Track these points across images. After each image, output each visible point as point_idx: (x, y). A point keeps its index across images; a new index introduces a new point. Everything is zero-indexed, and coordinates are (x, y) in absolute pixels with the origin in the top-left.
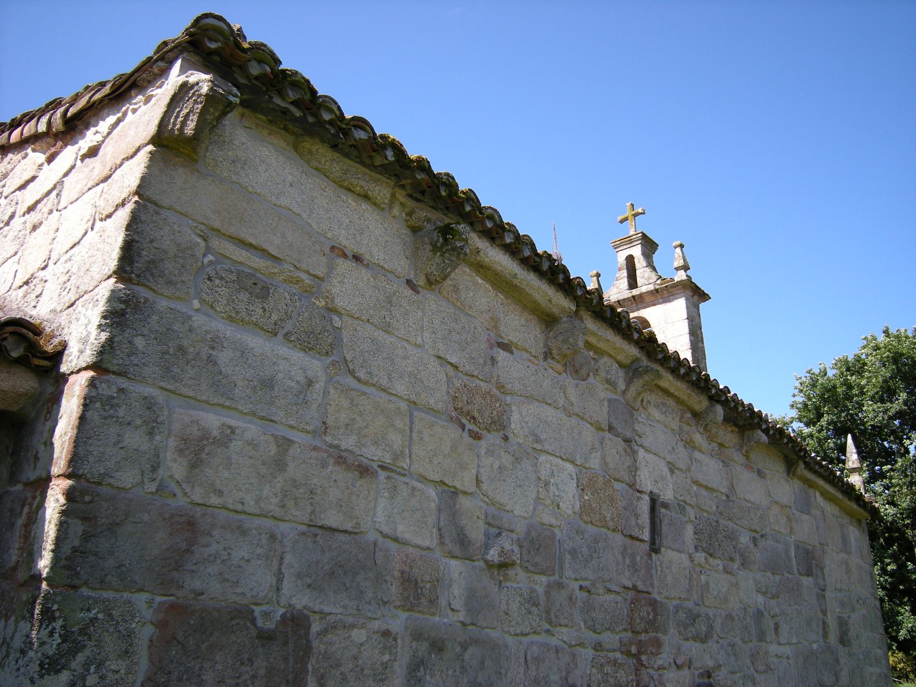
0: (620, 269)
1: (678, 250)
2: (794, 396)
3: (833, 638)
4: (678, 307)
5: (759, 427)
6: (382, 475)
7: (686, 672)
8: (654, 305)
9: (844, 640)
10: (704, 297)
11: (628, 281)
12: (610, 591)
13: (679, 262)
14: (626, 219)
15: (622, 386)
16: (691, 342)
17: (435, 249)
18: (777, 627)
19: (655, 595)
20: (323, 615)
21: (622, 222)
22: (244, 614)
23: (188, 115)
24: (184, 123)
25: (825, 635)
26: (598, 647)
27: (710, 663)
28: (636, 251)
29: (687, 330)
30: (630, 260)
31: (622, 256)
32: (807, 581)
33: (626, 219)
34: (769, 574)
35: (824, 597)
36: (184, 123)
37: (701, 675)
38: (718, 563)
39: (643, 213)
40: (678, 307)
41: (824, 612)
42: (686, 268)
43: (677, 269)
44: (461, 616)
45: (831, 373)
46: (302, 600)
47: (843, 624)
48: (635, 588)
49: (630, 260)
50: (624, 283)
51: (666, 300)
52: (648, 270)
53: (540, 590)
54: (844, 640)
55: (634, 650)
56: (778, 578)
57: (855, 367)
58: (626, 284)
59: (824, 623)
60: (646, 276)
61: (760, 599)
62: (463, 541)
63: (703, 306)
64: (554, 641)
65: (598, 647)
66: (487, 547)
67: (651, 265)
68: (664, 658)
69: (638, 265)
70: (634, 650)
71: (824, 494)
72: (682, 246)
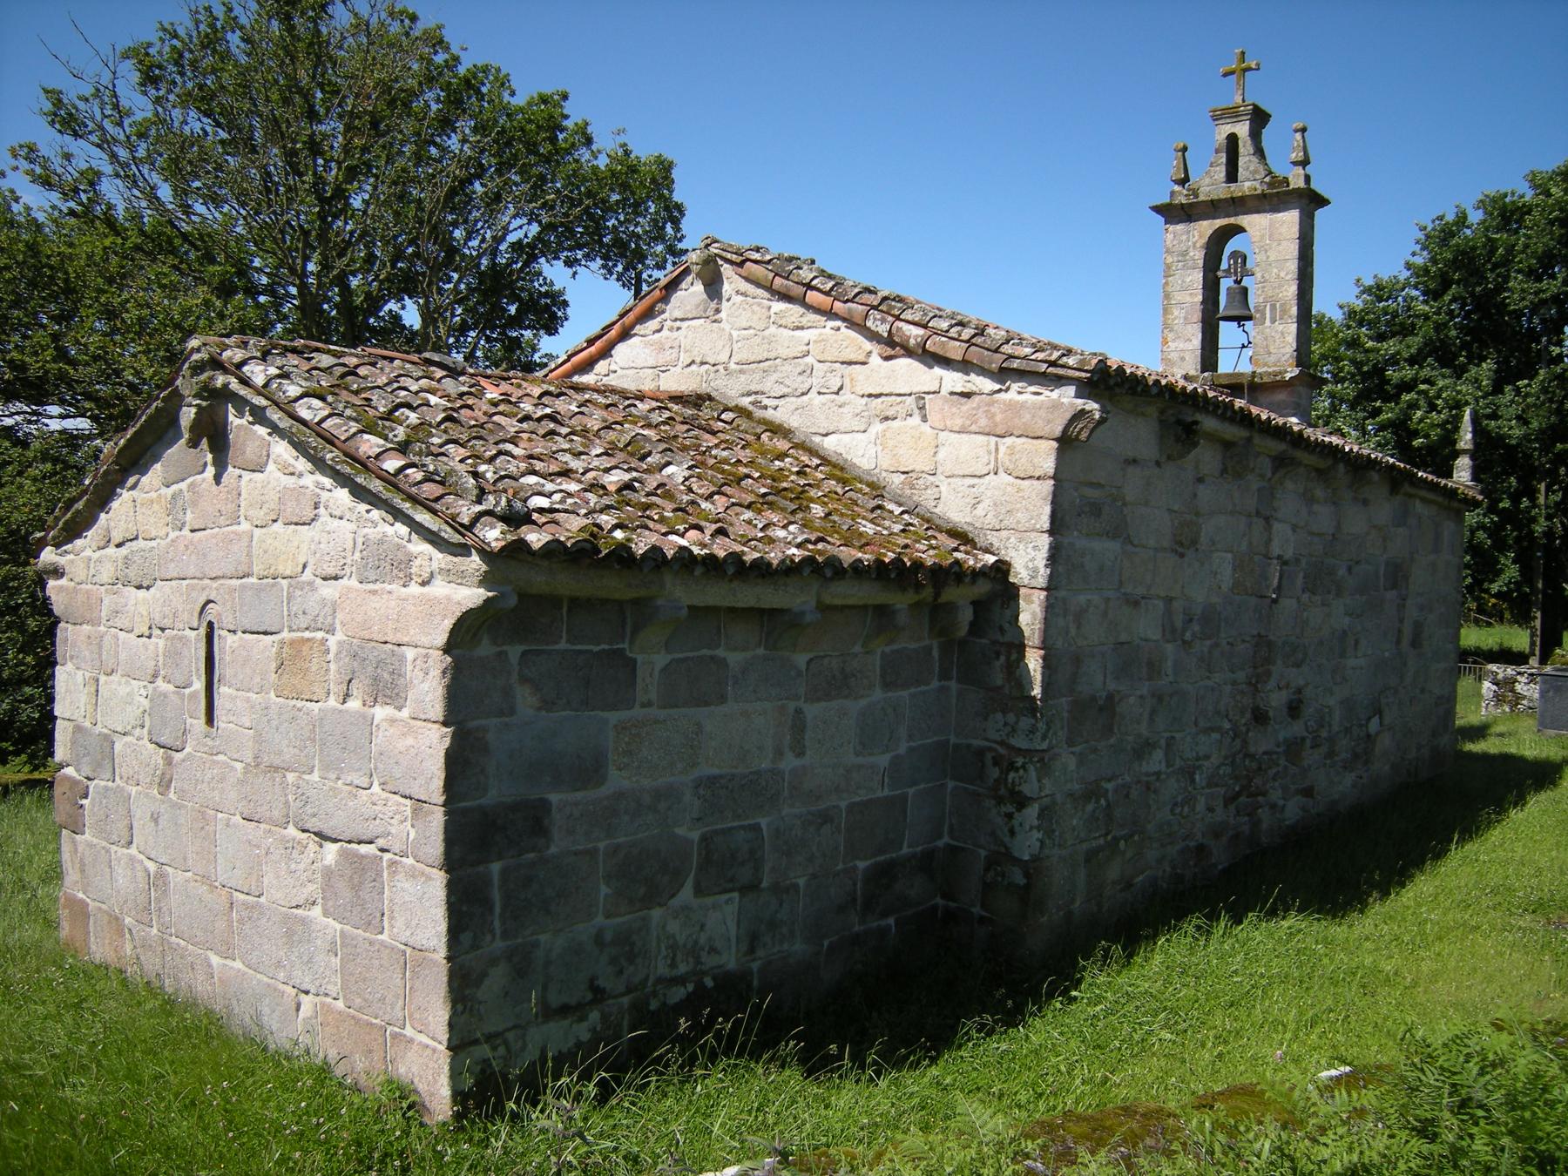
0: (1217, 151)
1: (1298, 136)
2: (1414, 254)
3: (1405, 642)
4: (1289, 220)
5: (1373, 468)
6: (1143, 602)
7: (1284, 692)
8: (1258, 212)
9: (1415, 643)
10: (1320, 201)
11: (1227, 171)
12: (1243, 641)
13: (1298, 155)
14: (1232, 73)
15: (1269, 475)
16: (1299, 268)
17: (1178, 440)
18: (1357, 642)
19: (1272, 637)
20: (1119, 692)
21: (1225, 75)
22: (1093, 699)
23: (1082, 429)
24: (1079, 433)
25: (1398, 642)
26: (1234, 683)
27: (1302, 682)
28: (1242, 129)
29: (1296, 253)
30: (1232, 140)
31: (1226, 129)
32: (1391, 595)
33: (1232, 73)
34: (1358, 597)
35: (1404, 606)
36: (1079, 433)
37: (1294, 693)
38: (1318, 598)
39: (1258, 69)
40: (1289, 220)
41: (1401, 621)
42: (1305, 163)
43: (1295, 163)
44: (1171, 679)
45: (1475, 217)
46: (1112, 686)
47: (1418, 627)
48: (1259, 635)
49: (1232, 140)
50: (1220, 173)
51: (1276, 209)
52: (1255, 159)
53: (1205, 650)
54: (1415, 643)
55: (1254, 681)
56: (1364, 598)
57: (1506, 214)
58: (1223, 174)
59: (1400, 631)
60: (1252, 168)
61: (1347, 620)
62: (1173, 631)
63: (1320, 214)
64: (1210, 683)
65: (1234, 683)
66: (1184, 630)
67: (1259, 152)
68: (1272, 683)
69: (1241, 150)
70: (1254, 681)
71: (1423, 500)
72: (1303, 130)
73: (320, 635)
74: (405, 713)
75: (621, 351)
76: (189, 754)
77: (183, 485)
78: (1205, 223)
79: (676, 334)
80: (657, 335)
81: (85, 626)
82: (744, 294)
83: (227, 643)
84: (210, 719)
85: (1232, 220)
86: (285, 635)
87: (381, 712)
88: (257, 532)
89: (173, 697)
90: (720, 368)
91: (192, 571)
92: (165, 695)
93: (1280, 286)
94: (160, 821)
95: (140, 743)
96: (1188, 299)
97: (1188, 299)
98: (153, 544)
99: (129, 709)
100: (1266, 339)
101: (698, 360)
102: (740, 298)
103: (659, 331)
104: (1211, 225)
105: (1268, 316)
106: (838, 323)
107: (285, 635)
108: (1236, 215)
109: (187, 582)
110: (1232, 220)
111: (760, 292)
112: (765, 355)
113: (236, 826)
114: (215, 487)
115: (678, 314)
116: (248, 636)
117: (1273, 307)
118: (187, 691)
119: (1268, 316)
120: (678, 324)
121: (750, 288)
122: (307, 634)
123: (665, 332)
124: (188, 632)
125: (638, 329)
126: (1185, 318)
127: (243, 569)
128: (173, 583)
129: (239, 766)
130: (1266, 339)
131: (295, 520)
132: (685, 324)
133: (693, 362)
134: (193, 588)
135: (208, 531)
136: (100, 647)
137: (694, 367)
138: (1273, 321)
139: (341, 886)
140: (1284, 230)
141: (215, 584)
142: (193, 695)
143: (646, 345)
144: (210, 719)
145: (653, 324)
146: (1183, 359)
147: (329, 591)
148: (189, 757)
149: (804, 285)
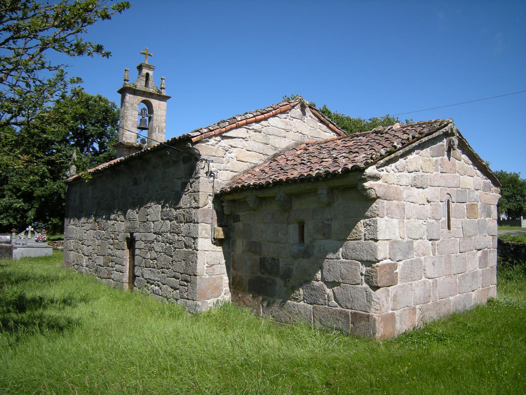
73: (476, 203)
74: (491, 219)
75: (272, 120)
76: (442, 240)
77: (439, 158)
78: (140, 97)
79: (291, 121)
80: (285, 119)
81: (394, 201)
82: (311, 117)
83: (452, 205)
84: (449, 228)
85: (148, 99)
86: (468, 203)
87: (487, 219)
88: (461, 177)
89: (435, 223)
90: (306, 136)
91: (443, 185)
92: (433, 223)
93: (161, 123)
94: (435, 264)
95: (424, 241)
96: (133, 119)
97: (133, 119)
98: (426, 174)
99: (421, 230)
100: (157, 137)
101: (299, 132)
102: (310, 118)
103: (285, 118)
104: (141, 98)
105: (157, 130)
106: (334, 134)
107: (468, 203)
108: (149, 98)
109: (441, 188)
110: (148, 99)
111: (316, 118)
112: (318, 136)
113: (459, 255)
114: (448, 162)
115: (293, 115)
116: (458, 204)
117: (159, 128)
118: (440, 221)
119: (157, 130)
120: (292, 118)
121: (312, 115)
122: (473, 203)
123: (287, 120)
124: (440, 203)
125: (279, 115)
126: (132, 125)
127: (458, 186)
128: (436, 187)
129: (458, 239)
130: (157, 137)
131: (470, 175)
132: (295, 120)
133: (298, 132)
134: (443, 189)
135: (447, 174)
136: (404, 209)
137: (297, 133)
138: (159, 132)
139: (482, 259)
140: (162, 107)
141: (449, 189)
142: (443, 222)
143: (282, 121)
144: (449, 228)
145: (284, 116)
146: (131, 138)
147: (477, 193)
148: (442, 241)
149: (406, 133)
